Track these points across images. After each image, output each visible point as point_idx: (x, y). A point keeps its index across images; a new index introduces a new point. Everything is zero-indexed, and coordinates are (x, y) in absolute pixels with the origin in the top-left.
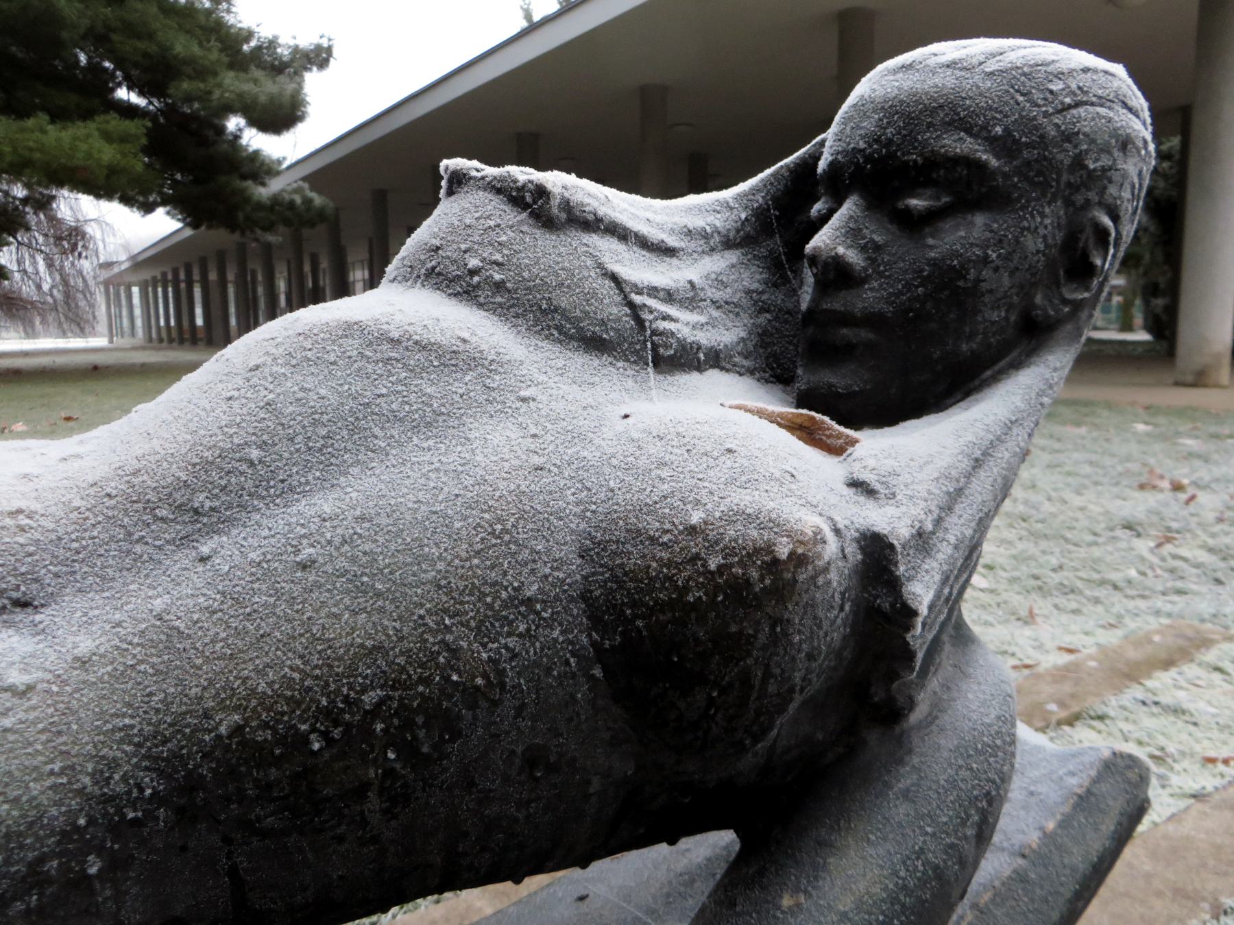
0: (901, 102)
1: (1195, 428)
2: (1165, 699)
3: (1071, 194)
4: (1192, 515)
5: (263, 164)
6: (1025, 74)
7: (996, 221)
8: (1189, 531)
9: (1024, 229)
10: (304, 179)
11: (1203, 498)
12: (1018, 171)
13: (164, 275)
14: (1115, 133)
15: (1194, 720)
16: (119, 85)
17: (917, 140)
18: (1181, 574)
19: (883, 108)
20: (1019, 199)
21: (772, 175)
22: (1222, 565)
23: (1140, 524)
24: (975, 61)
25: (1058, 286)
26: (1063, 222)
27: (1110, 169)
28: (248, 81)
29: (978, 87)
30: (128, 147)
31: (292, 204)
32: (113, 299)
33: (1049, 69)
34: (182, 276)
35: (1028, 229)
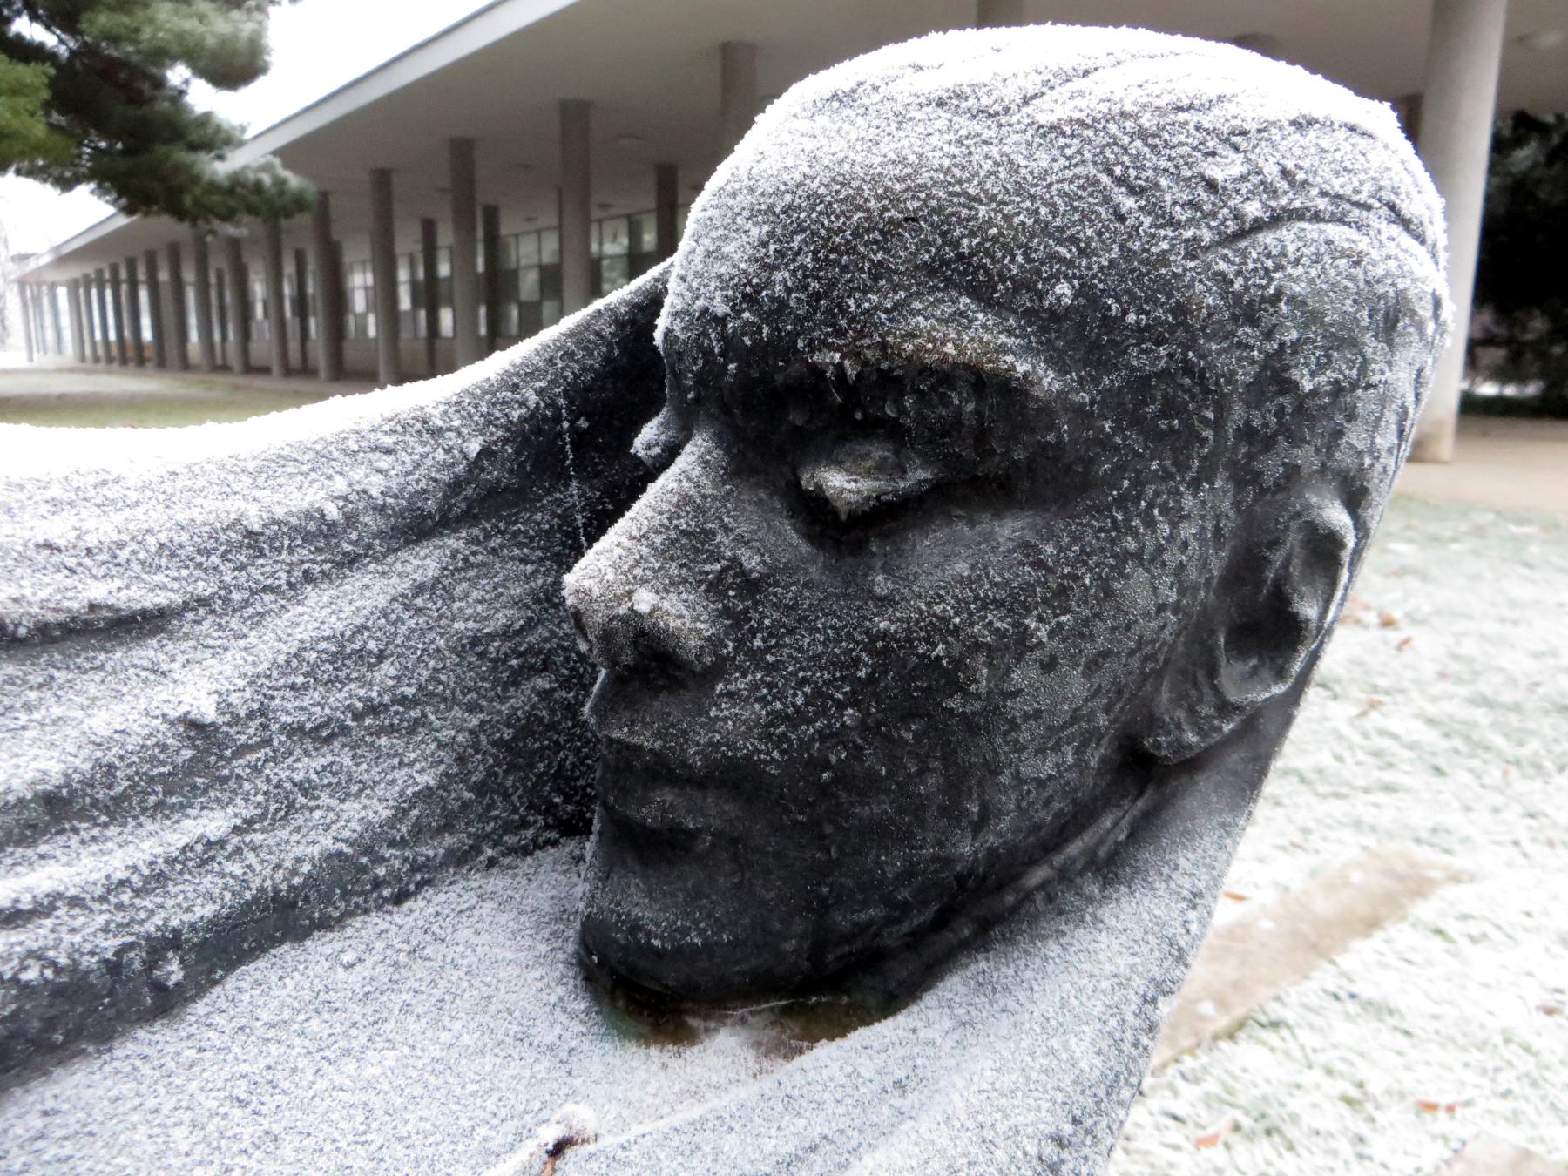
0: (815, 198)
1: (1409, 527)
2: (1366, 991)
3: (1250, 457)
4: (1406, 666)
5: (218, 129)
6: (1142, 134)
7: (1052, 536)
8: (1402, 691)
9: (1127, 555)
10: (275, 153)
11: (1423, 640)
12: (1110, 401)
13: (100, 272)
14: (1368, 296)
15: (1405, 1026)
16: (19, 13)
17: (844, 310)
18: (1390, 759)
19: (771, 208)
20: (1112, 480)
21: (571, 334)
22: (1444, 744)
23: (1338, 681)
24: (1012, 94)
25: (1212, 672)
26: (1228, 526)
27: (1354, 386)
28: (190, 16)
29: (1014, 169)
30: (21, 102)
31: (258, 187)
32: (31, 304)
33: (1207, 120)
34: (123, 274)
35: (1138, 556)
